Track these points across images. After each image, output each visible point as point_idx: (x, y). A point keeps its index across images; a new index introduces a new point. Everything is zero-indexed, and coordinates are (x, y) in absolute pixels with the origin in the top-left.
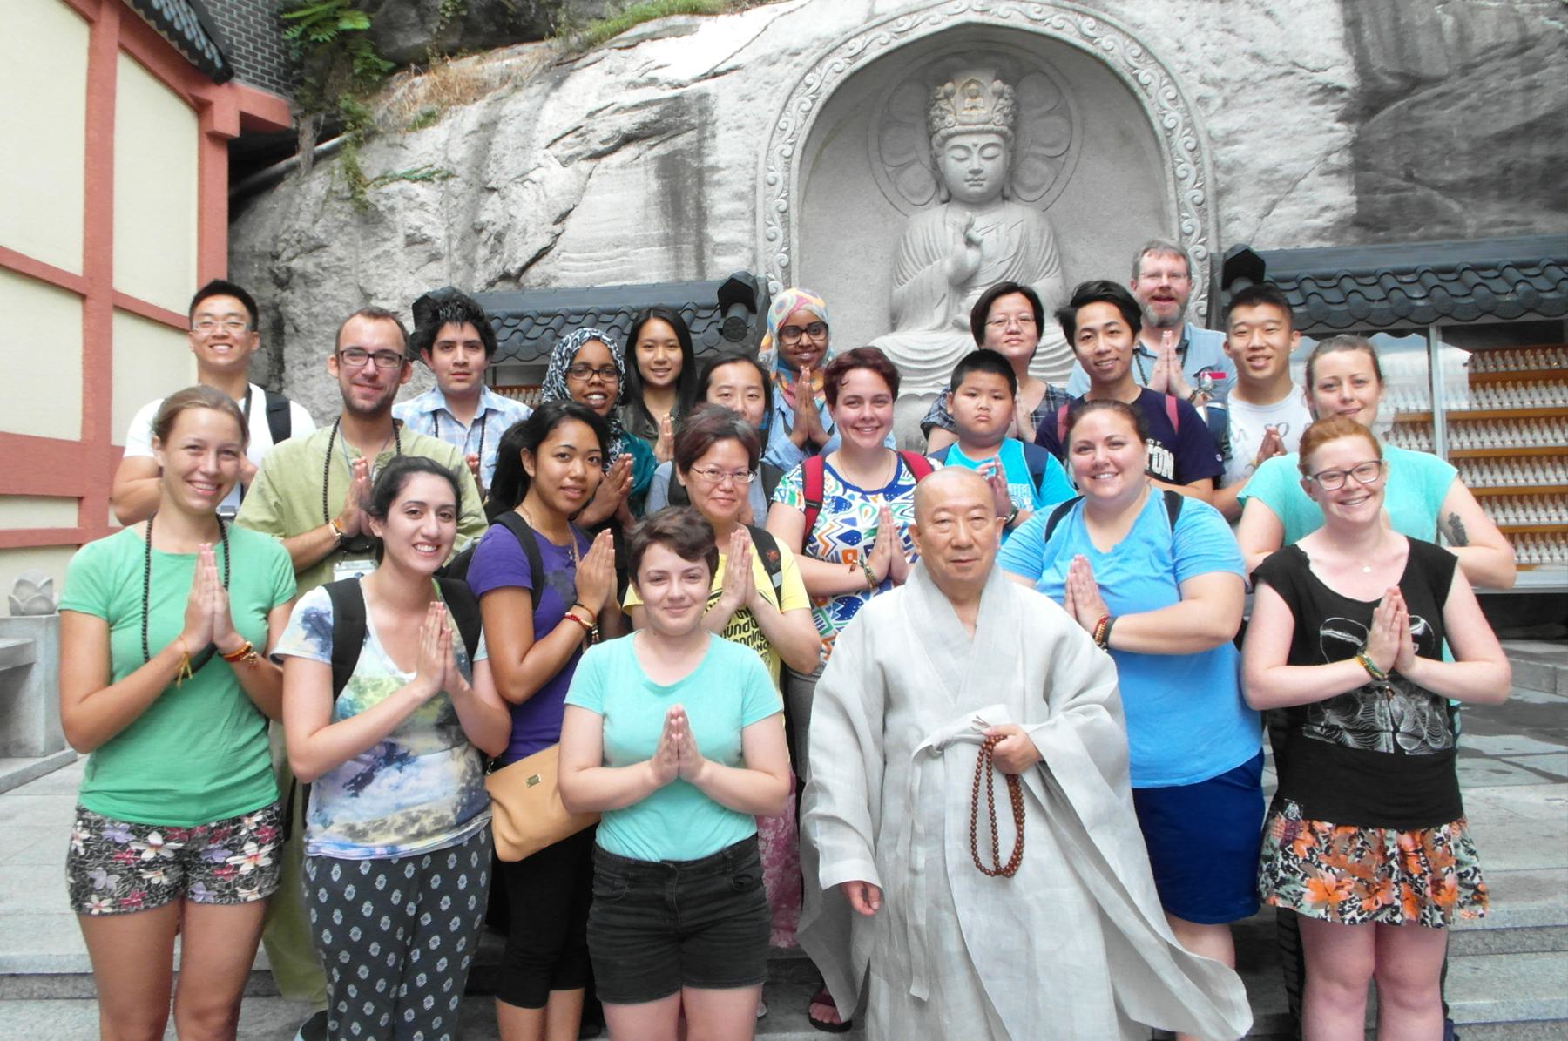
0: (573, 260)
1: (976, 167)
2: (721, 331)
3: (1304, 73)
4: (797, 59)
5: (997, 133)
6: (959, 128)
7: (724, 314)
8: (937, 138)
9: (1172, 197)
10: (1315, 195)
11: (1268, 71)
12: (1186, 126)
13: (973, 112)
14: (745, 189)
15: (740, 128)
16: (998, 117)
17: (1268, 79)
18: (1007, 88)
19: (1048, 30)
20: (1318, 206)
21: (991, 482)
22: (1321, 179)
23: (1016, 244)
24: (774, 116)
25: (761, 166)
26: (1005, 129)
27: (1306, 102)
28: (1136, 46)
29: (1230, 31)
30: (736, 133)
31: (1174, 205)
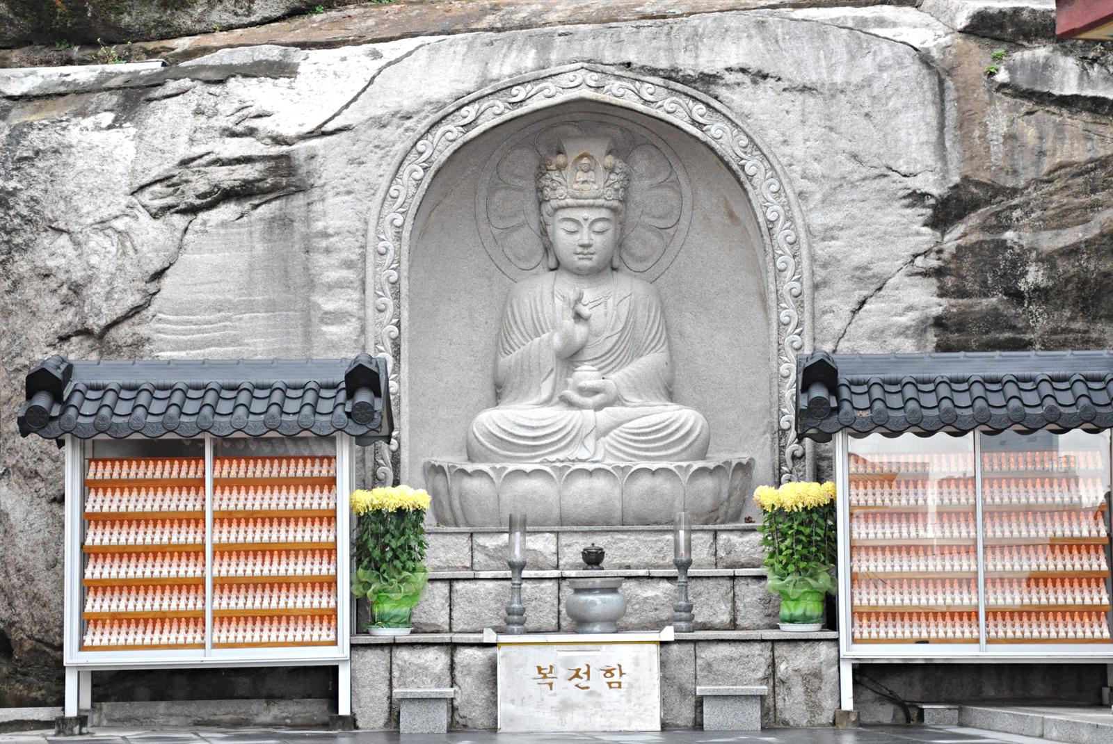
0: (169, 322)
1: (586, 242)
2: (349, 414)
3: (896, 176)
4: (408, 123)
5: (608, 208)
6: (570, 201)
7: (350, 396)
8: (547, 208)
9: (772, 287)
10: (901, 294)
11: (865, 171)
12: (787, 219)
13: (582, 192)
14: (354, 257)
15: (349, 193)
16: (610, 193)
17: (864, 179)
18: (620, 164)
19: (661, 114)
20: (904, 305)
21: (149, 339)
22: (907, 279)
23: (623, 318)
24: (384, 182)
25: (371, 234)
26: (615, 203)
27: (897, 204)
28: (742, 136)
29: (831, 129)
30: (346, 198)
31: (773, 296)
